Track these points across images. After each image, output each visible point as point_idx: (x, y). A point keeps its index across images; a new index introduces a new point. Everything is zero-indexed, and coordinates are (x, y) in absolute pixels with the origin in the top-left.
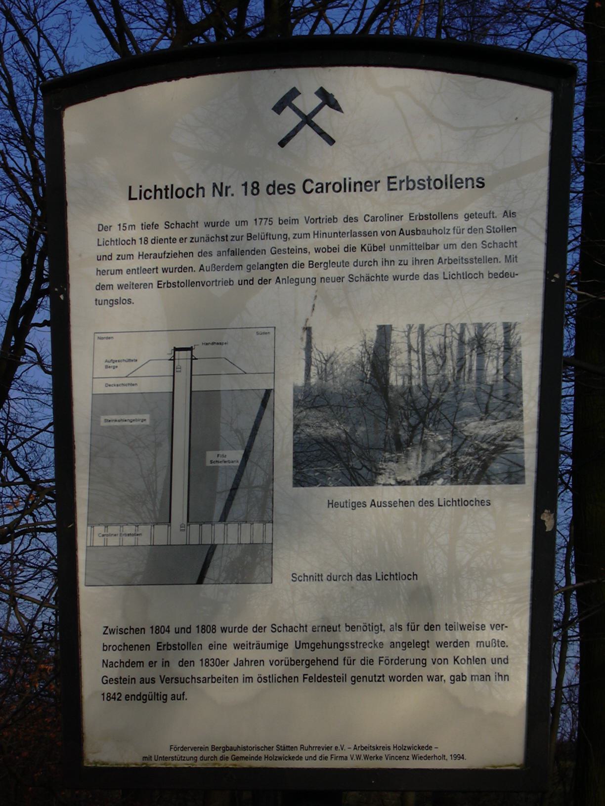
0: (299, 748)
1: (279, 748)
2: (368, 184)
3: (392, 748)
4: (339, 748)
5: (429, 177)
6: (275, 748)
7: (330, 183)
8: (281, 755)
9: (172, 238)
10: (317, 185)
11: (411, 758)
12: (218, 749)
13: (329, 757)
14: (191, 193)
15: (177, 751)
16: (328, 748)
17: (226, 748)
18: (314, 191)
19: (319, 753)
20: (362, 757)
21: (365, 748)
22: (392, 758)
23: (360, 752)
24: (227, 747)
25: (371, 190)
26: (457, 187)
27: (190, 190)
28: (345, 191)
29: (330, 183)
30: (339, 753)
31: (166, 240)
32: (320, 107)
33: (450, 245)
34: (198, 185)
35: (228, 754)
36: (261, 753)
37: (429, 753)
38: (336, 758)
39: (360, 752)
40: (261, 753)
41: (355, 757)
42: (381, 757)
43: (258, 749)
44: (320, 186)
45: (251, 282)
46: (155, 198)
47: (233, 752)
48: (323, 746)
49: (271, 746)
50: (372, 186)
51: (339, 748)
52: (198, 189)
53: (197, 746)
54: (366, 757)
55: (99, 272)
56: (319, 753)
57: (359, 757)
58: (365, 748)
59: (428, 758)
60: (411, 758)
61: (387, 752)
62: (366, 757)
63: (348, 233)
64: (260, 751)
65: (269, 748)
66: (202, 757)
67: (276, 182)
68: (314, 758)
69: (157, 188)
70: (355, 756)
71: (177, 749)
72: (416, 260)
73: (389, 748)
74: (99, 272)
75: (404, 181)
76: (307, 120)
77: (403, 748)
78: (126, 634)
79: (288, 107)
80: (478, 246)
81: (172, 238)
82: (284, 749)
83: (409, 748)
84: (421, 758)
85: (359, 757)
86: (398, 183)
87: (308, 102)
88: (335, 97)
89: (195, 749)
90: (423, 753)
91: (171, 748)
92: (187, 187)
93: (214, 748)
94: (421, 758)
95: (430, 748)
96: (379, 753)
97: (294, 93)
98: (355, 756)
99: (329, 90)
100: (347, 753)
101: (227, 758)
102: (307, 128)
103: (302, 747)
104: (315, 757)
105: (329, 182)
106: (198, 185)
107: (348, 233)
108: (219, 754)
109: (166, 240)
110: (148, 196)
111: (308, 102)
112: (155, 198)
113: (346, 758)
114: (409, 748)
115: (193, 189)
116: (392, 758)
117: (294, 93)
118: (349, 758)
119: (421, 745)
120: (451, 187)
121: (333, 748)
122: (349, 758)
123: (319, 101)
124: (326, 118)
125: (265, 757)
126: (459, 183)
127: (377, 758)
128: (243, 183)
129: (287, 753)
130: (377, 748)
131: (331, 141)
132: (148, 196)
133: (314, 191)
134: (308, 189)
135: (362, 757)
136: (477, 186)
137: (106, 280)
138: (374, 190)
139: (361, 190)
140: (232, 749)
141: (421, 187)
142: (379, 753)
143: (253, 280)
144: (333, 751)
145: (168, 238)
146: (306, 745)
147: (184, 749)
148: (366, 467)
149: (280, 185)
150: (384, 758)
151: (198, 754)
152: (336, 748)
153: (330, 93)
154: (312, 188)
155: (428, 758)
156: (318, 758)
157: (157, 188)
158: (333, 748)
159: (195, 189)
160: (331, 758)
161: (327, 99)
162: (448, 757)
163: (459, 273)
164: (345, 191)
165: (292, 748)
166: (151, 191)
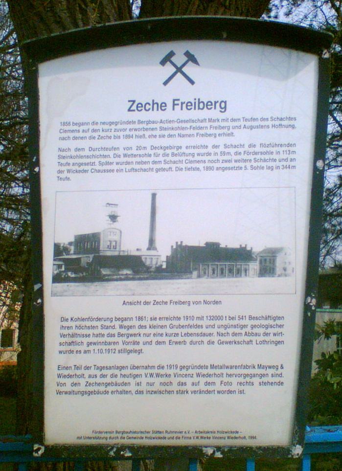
1: (154, 432)
2: (189, 104)
7: (184, 103)
8: (96, 341)
12: (119, 433)
14: (148, 107)
16: (181, 432)
17: (123, 432)
20: (155, 375)
21: (201, 432)
25: (191, 109)
26: (162, 110)
27: (147, 105)
29: (184, 103)
30: (188, 435)
32: (184, 65)
34: (153, 101)
35: (125, 435)
36: (144, 435)
37: (237, 435)
38: (185, 438)
40: (144, 435)
41: (148, 375)
42: (210, 438)
46: (153, 110)
47: (128, 435)
50: (212, 105)
51: (187, 432)
52: (153, 104)
54: (202, 437)
56: (175, 435)
57: (197, 438)
58: (201, 432)
59: (236, 438)
61: (214, 435)
62: (202, 437)
65: (148, 432)
68: (173, 438)
69: (155, 102)
70: (149, 374)
71: (96, 433)
73: (215, 432)
76: (179, 70)
77: (223, 432)
78: (64, 345)
79: (168, 62)
83: (226, 433)
85: (197, 438)
86: (180, 104)
88: (223, 245)
92: (146, 102)
93: (117, 432)
94: (232, 438)
95: (237, 432)
97: (172, 54)
98: (149, 374)
99: (192, 53)
101: (124, 438)
102: (179, 75)
103: (166, 432)
105: (216, 101)
106: (153, 101)
108: (120, 435)
110: (147, 108)
111: (179, 59)
112: (153, 110)
114: (226, 433)
115: (149, 104)
116: (216, 438)
117: (172, 54)
124: (189, 69)
126: (140, 107)
128: (257, 437)
131: (165, 83)
132: (147, 108)
135: (155, 375)
138: (213, 108)
139: (158, 110)
140: (127, 432)
146: (169, 431)
147: (100, 432)
149: (162, 103)
151: (108, 435)
152: (185, 432)
153: (202, 244)
155: (236, 438)
156: (175, 438)
157: (155, 102)
161: (191, 58)
162: (247, 437)
165: (160, 432)
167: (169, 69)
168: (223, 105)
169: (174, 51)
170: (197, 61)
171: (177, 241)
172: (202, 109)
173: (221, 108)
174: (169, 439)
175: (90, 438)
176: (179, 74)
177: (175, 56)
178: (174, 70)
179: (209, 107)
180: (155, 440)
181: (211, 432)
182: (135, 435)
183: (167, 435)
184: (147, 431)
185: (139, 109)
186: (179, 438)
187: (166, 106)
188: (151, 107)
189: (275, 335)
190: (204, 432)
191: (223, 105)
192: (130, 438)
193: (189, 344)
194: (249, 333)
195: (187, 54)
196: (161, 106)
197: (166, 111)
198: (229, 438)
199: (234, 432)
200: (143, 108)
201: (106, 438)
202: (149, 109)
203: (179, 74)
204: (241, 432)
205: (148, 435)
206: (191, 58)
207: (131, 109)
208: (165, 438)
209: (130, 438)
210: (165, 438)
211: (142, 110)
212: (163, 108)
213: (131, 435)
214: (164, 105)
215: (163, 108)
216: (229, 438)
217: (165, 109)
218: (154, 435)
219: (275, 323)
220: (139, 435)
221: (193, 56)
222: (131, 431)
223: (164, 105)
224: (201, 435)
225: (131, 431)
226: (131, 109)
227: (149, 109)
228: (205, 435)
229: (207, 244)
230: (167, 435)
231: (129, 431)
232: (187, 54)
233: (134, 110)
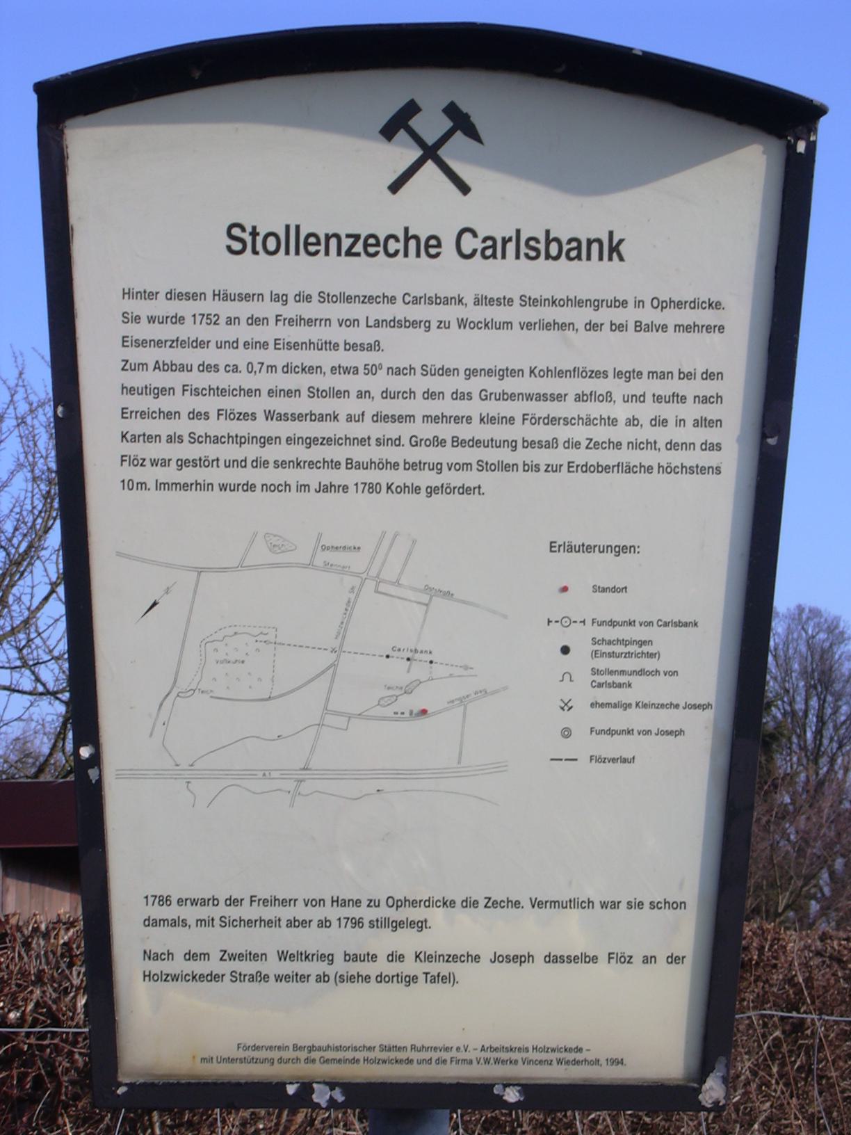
0: (409, 1049)
1: (383, 1048)
3: (531, 1050)
4: (462, 1049)
5: (254, 228)
6: (377, 1049)
8: (386, 1058)
9: (148, 291)
10: (484, 240)
11: (555, 1062)
12: (301, 1048)
13: (449, 1061)
14: (393, 245)
15: (247, 1052)
16: (447, 1049)
17: (312, 1048)
18: (479, 253)
19: (435, 1055)
20: (492, 1061)
21: (496, 1050)
22: (530, 1062)
23: (488, 1055)
24: (313, 1046)
25: (317, 252)
28: (287, 253)
30: (461, 1056)
31: (568, 373)
33: (504, 323)
35: (316, 1055)
36: (359, 1055)
37: (579, 1056)
39: (488, 1055)
41: (482, 1061)
42: (516, 1062)
43: (356, 1049)
44: (489, 243)
45: (235, 345)
46: (406, 255)
47: (321, 1053)
48: (441, 1045)
49: (373, 1046)
51: (462, 1049)
53: (274, 1045)
54: (497, 1061)
55: (125, 390)
57: (487, 1061)
59: (576, 1062)
60: (555, 1062)
61: (524, 1055)
62: (497, 1061)
63: (535, 324)
64: (358, 1052)
65: (370, 1049)
66: (281, 1058)
67: (522, 233)
69: (410, 235)
71: (246, 1048)
72: (301, 320)
73: (527, 1050)
74: (125, 390)
75: (510, 239)
76: (430, 152)
77: (545, 1050)
79: (402, 130)
80: (265, 298)
81: (148, 291)
82: (390, 1050)
83: (553, 1050)
84: (567, 1062)
85: (487, 1061)
87: (431, 124)
89: (271, 1048)
90: (570, 1056)
91: (238, 1048)
93: (296, 1047)
94: (567, 1062)
95: (579, 1050)
96: (514, 1056)
97: (411, 109)
99: (465, 108)
100: (471, 1055)
103: (413, 1047)
104: (431, 1059)
107: (535, 324)
109: (568, 373)
110: (391, 250)
111: (431, 124)
113: (471, 1062)
114: (553, 1050)
116: (530, 1062)
117: (411, 109)
118: (475, 1062)
119: (568, 1046)
120: (297, 253)
121: (454, 1049)
122: (475, 1062)
123: (448, 124)
125: (364, 1060)
127: (511, 1062)
129: (393, 1055)
130: (511, 1050)
131: (395, 187)
132: (391, 250)
133: (479, 253)
134: (467, 250)
135: (492, 1061)
136: (527, 256)
137: (136, 355)
140: (320, 1049)
141: (533, 254)
142: (514, 1056)
143: (237, 342)
144: (454, 1053)
145: (142, 291)
147: (256, 1048)
148: (392, 583)
150: (520, 1062)
152: (458, 1049)
153: (465, 112)
154: (475, 247)
155: (576, 1062)
156: (433, 1061)
157: (410, 235)
158: (454, 1049)
159: (543, 240)
160: (451, 1061)
161: (461, 122)
162: (603, 1061)
163: (550, 368)
164: (287, 253)
165: (399, 1049)
166: (397, 240)
167: (403, 153)
168: (427, 324)
169: (419, 102)
170: (479, 137)
171: (333, 894)
172: (283, 295)
173: (154, 394)
174: (420, 1062)
175: (231, 1060)
176: (430, 165)
177: (421, 113)
178: (417, 153)
179: (312, 249)
180: (387, 1066)
181: (519, 1049)
182: (339, 1055)
183: (415, 1056)
184: (368, 1045)
185: (372, 250)
186: (444, 1061)
187: (439, 245)
188: (400, 246)
189: (579, 398)
190: (503, 1049)
191: (427, 324)
192: (327, 1061)
193: (457, 902)
194: (164, 365)
195: (452, 111)
196: (427, 246)
197: (438, 258)
198: (559, 1062)
199: (570, 1050)
200: (381, 249)
201: (272, 1062)
202: (397, 252)
203: (430, 165)
204: (588, 1050)
205: (371, 1055)
206: (461, 122)
207: (354, 250)
208: (410, 1061)
209: (327, 1061)
210: (410, 1061)
211: (376, 253)
212: (433, 251)
213: (330, 1055)
214: (433, 242)
215: (433, 251)
216: (559, 1062)
217: (438, 255)
218: (384, 1055)
219: (639, 650)
220: (350, 1055)
221: (467, 117)
222: (328, 1046)
223: (433, 242)
224: (496, 1055)
225: (328, 1046)
226: (354, 250)
227: (397, 252)
228: (504, 1056)
229: (467, 114)
230: (415, 1056)
231: (324, 1044)
232: (452, 111)
233: (358, 254)
